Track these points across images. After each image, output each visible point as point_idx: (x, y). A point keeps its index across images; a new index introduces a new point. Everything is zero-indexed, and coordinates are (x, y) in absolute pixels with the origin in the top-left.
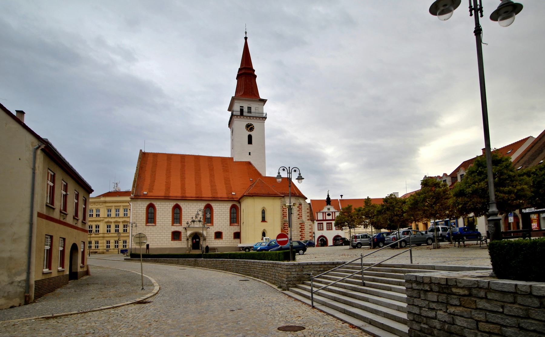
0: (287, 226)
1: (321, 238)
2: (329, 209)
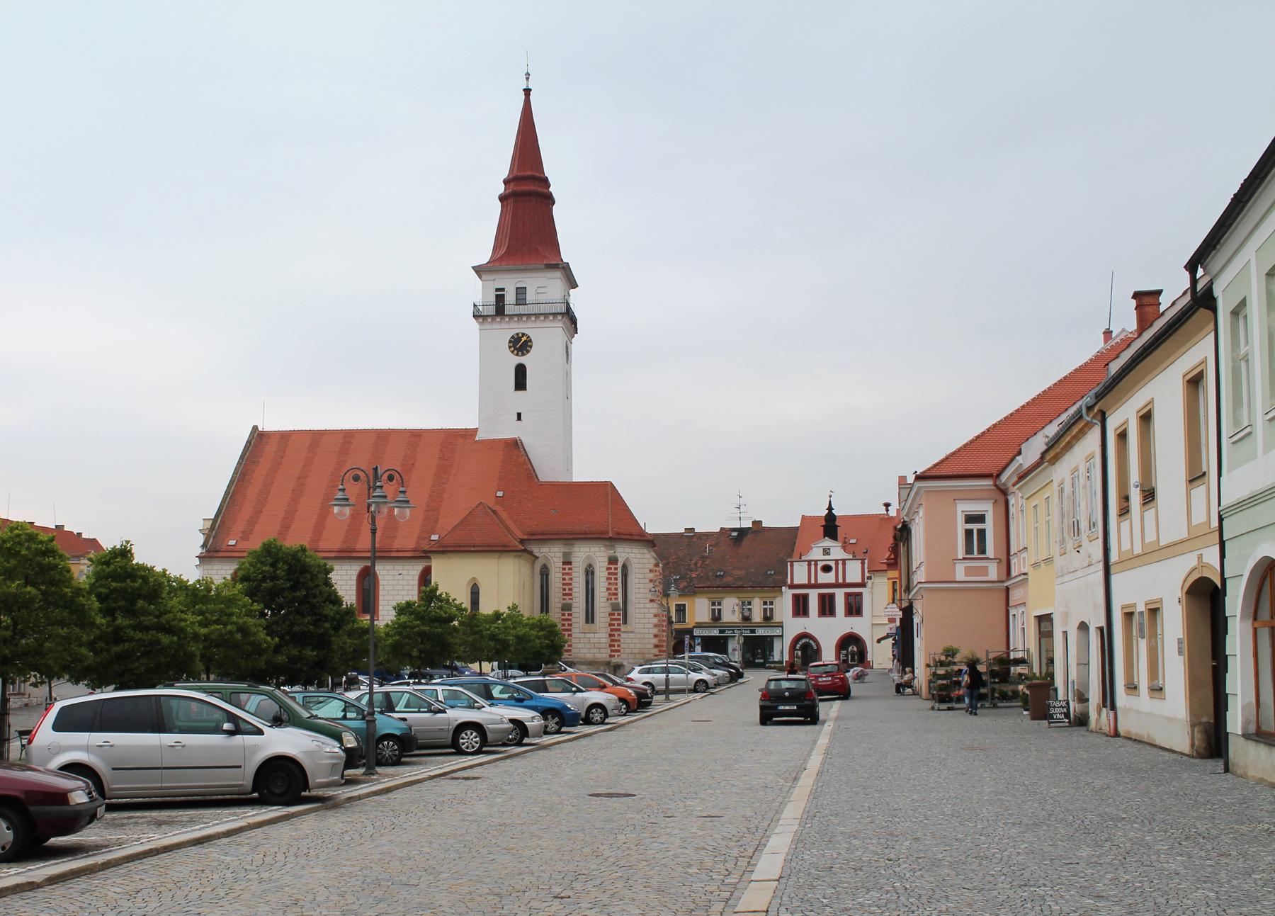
0: (619, 619)
1: (804, 641)
2: (826, 552)
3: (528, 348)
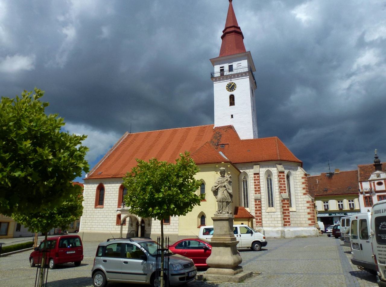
3: (235, 88)
